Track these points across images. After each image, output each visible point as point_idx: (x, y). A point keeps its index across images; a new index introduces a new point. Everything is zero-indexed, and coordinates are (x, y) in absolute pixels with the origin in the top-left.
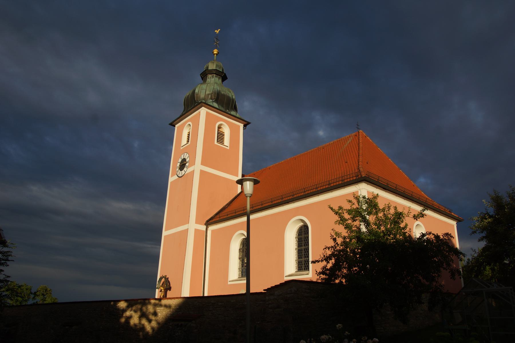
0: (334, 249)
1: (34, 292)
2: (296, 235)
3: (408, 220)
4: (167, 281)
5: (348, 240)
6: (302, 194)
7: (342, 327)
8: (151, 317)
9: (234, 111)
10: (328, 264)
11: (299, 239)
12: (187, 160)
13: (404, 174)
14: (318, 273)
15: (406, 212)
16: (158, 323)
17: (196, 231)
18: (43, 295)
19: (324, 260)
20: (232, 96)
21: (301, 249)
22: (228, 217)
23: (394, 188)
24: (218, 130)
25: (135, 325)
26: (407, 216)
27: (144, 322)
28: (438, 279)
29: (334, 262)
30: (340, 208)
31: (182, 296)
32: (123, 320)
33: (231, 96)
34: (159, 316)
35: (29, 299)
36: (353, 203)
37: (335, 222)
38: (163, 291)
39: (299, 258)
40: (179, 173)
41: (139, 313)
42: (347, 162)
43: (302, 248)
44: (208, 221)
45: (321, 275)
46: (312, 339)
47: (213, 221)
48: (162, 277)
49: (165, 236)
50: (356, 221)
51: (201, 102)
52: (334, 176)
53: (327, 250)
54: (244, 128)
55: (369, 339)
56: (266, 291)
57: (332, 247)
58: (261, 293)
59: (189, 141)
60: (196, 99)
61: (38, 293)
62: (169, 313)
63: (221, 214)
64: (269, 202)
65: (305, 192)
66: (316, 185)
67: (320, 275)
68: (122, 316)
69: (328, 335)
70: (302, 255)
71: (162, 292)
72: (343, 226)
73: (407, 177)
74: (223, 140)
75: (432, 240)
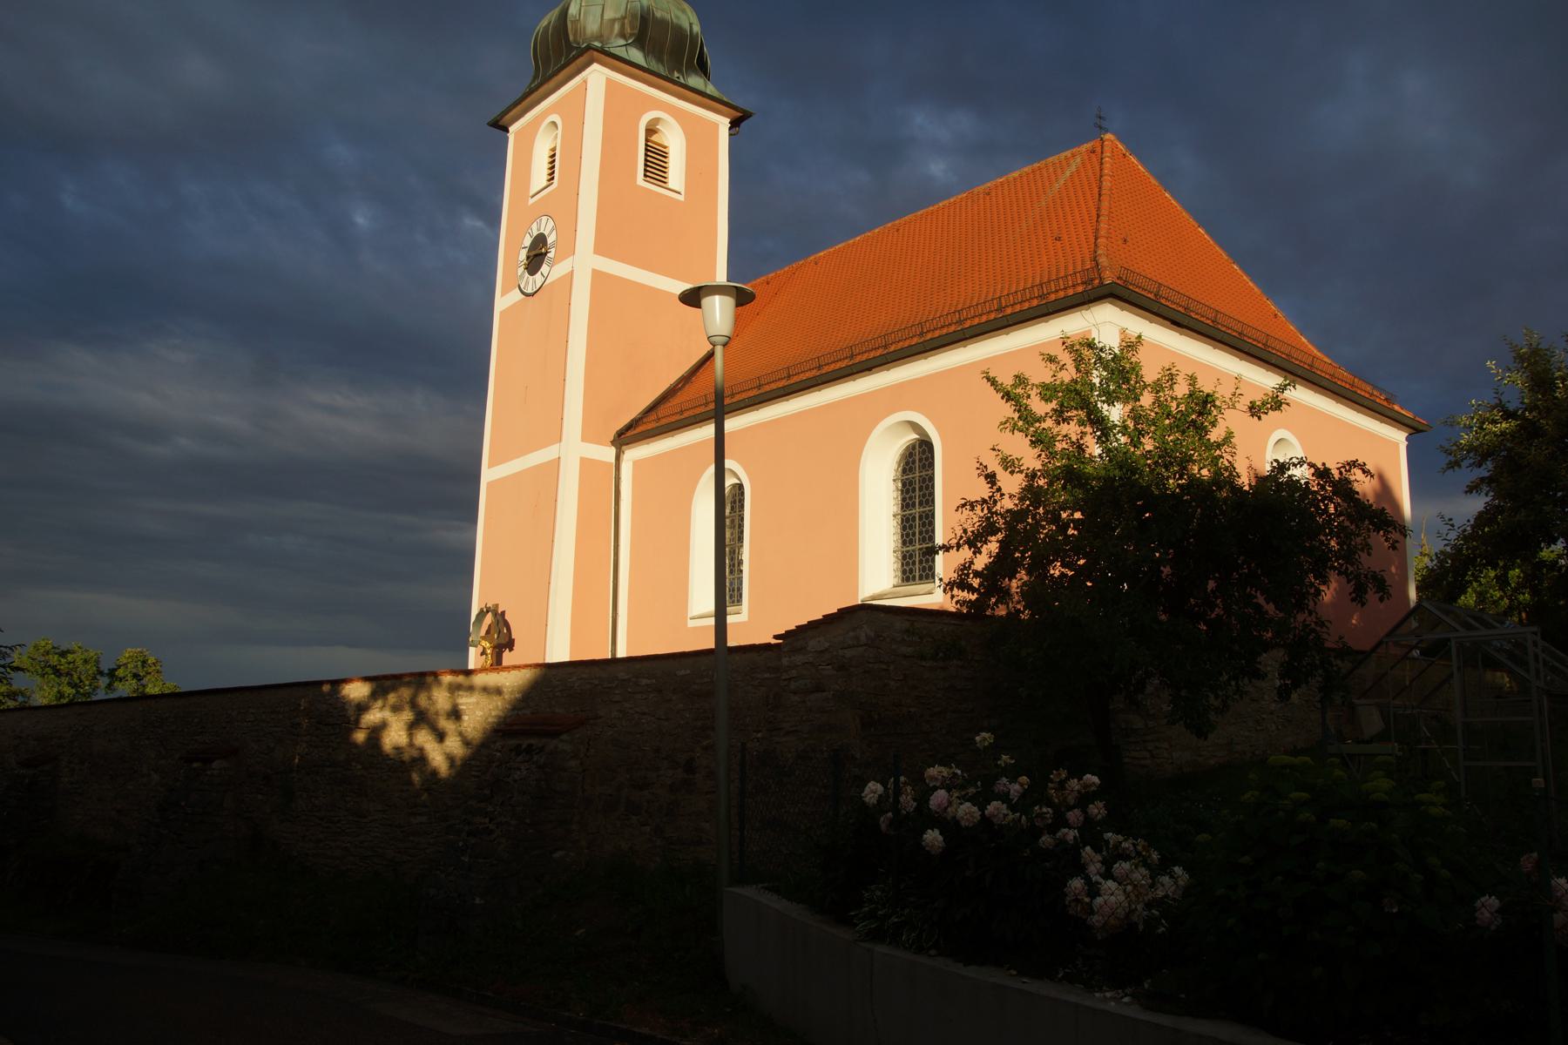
0: (988, 508)
1: (109, 670)
2: (897, 471)
3: (1230, 422)
4: (501, 620)
5: (1042, 482)
6: (915, 340)
7: (992, 741)
8: (444, 723)
9: (697, 74)
10: (978, 555)
11: (904, 485)
12: (550, 241)
13: (1245, 277)
14: (947, 585)
15: (1223, 392)
16: (466, 743)
17: (585, 463)
18: (136, 676)
19: (966, 542)
20: (691, 24)
21: (910, 515)
22: (682, 417)
23: (1208, 322)
24: (647, 140)
25: (398, 749)
26: (1229, 408)
27: (424, 738)
28: (1316, 604)
29: (997, 551)
30: (1020, 380)
31: (547, 661)
32: (360, 736)
33: (686, 26)
34: (465, 724)
35: (94, 690)
36: (1062, 363)
37: (1001, 424)
38: (489, 651)
39: (904, 543)
40: (527, 283)
41: (407, 715)
42: (1058, 239)
43: (914, 511)
44: (620, 434)
45: (956, 591)
46: (902, 779)
47: (635, 432)
48: (485, 610)
49: (490, 484)
50: (1071, 422)
51: (589, 48)
52: (1018, 282)
53: (966, 512)
54: (733, 132)
55: (1073, 779)
56: (781, 641)
57: (984, 501)
58: (768, 646)
59: (553, 178)
60: (571, 38)
61: (120, 673)
62: (494, 713)
63: (662, 411)
64: (810, 370)
65: (922, 334)
66: (959, 311)
67: (952, 589)
68: (356, 724)
69: (951, 768)
70: (914, 534)
71: (487, 655)
72: (1026, 436)
73: (1256, 289)
74: (665, 172)
75: (1307, 483)
